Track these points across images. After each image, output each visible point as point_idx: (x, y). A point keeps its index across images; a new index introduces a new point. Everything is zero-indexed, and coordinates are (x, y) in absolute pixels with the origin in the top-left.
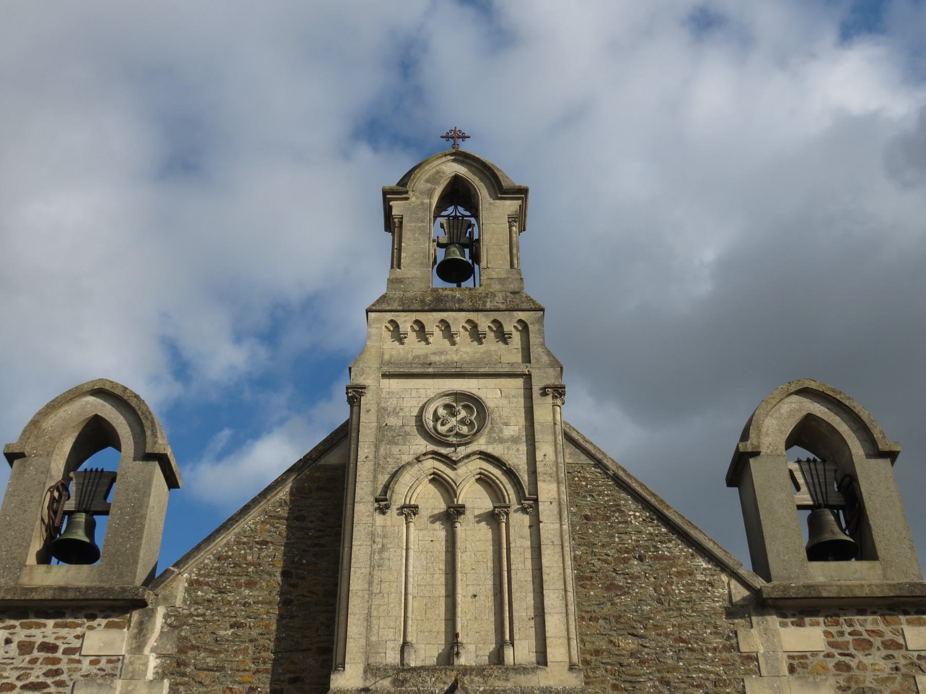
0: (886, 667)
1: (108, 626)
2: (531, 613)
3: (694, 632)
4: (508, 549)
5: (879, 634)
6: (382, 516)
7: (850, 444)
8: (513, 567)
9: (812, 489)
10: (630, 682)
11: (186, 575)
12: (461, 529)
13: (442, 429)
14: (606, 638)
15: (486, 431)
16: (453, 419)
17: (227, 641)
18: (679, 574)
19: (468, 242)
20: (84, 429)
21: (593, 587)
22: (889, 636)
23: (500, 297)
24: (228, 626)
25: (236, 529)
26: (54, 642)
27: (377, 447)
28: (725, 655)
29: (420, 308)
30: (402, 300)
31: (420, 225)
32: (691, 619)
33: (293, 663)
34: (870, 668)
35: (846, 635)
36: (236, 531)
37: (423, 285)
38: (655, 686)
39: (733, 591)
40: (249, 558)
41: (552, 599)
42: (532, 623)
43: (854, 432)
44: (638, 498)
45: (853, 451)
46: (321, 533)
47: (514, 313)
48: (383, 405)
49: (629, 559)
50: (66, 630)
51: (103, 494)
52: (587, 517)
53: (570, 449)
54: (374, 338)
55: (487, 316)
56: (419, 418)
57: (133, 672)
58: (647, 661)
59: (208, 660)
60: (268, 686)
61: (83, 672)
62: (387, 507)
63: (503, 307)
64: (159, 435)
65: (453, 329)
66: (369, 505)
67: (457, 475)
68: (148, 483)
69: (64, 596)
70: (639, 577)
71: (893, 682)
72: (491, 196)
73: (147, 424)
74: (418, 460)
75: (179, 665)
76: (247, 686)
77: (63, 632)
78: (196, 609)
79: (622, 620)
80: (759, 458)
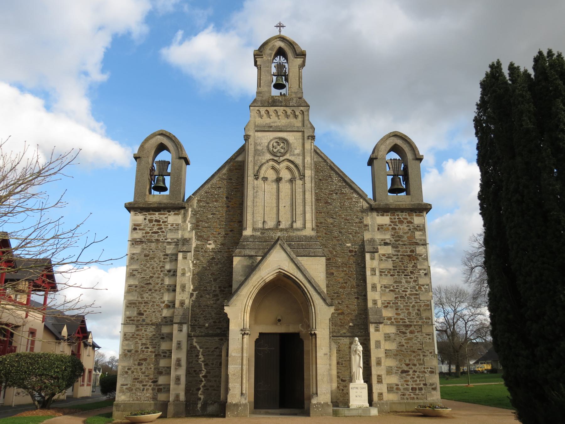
0: (407, 229)
1: (175, 214)
4: (295, 192)
5: (406, 219)
10: (330, 232)
11: (196, 198)
12: (281, 185)
13: (275, 150)
16: (279, 147)
18: (348, 199)
19: (284, 74)
21: (321, 202)
22: (409, 219)
23: (294, 101)
24: (210, 214)
26: (159, 219)
27: (254, 157)
28: (359, 224)
33: (231, 225)
34: (402, 229)
36: (211, 183)
39: (364, 205)
41: (308, 208)
44: (337, 173)
47: (299, 107)
48: (256, 142)
49: (333, 194)
52: (320, 180)
53: (316, 156)
55: (290, 109)
56: (268, 146)
58: (336, 226)
59: (206, 225)
61: (169, 228)
62: (258, 178)
63: (295, 105)
65: (279, 114)
68: (182, 164)
74: (267, 161)
75: (197, 226)
77: (161, 216)
80: (377, 160)
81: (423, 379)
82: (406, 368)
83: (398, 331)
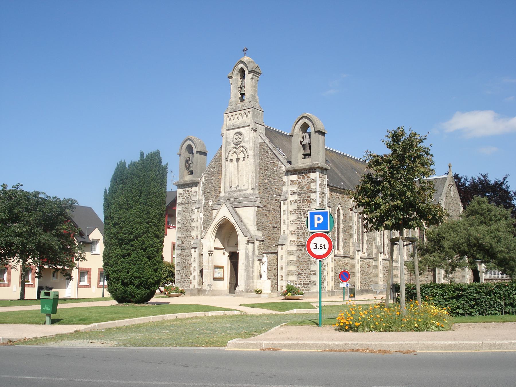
82: (301, 272)
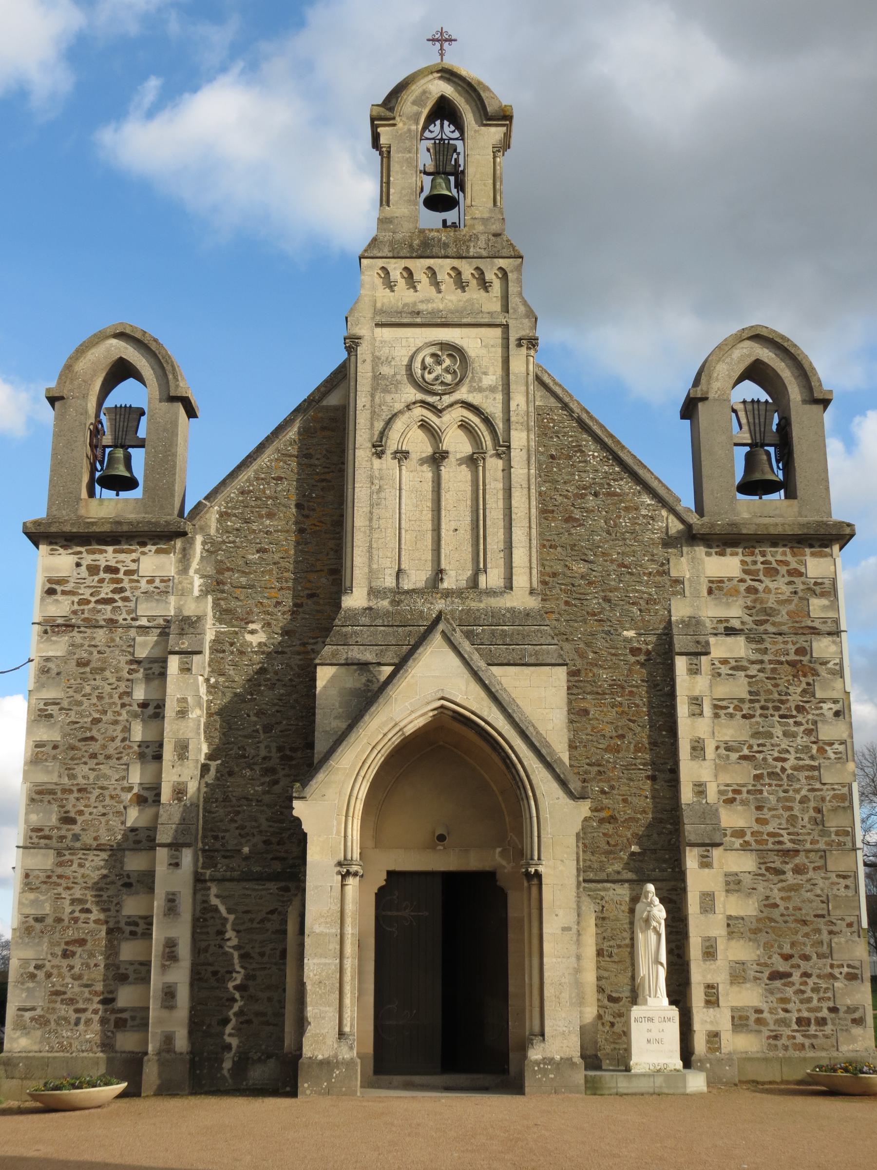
0: (787, 590)
1: (158, 552)
2: (501, 546)
3: (634, 559)
5: (786, 563)
6: (379, 460)
7: (790, 390)
8: (488, 506)
9: (752, 428)
10: (579, 599)
11: (216, 508)
13: (429, 377)
14: (562, 562)
15: (467, 381)
16: (439, 368)
17: (255, 563)
18: (627, 509)
19: (453, 170)
20: (110, 369)
21: (554, 519)
22: (794, 565)
23: (482, 243)
24: (255, 551)
25: (255, 466)
27: (373, 396)
28: (658, 578)
29: (408, 255)
30: (392, 243)
31: (408, 156)
32: (633, 548)
34: (773, 591)
35: (759, 563)
37: (411, 226)
38: (599, 603)
39: (670, 525)
40: (268, 492)
41: (519, 535)
42: (502, 554)
43: (796, 378)
44: (597, 439)
45: (792, 397)
46: (326, 470)
47: (496, 260)
48: (377, 354)
49: (586, 495)
50: (124, 555)
51: (134, 429)
53: (540, 393)
54: (367, 286)
56: (409, 367)
57: (183, 590)
59: (242, 579)
60: (290, 600)
62: (383, 452)
63: (484, 253)
64: (180, 378)
65: (439, 278)
66: (368, 450)
67: (441, 422)
68: (175, 423)
69: (119, 529)
70: (593, 511)
71: (790, 604)
72: (476, 123)
73: (168, 368)
74: (408, 407)
75: (218, 583)
76: (274, 600)
77: (122, 556)
78: (228, 537)
79: (576, 548)
80: (707, 402)
81: (829, 994)
83: (763, 867)
